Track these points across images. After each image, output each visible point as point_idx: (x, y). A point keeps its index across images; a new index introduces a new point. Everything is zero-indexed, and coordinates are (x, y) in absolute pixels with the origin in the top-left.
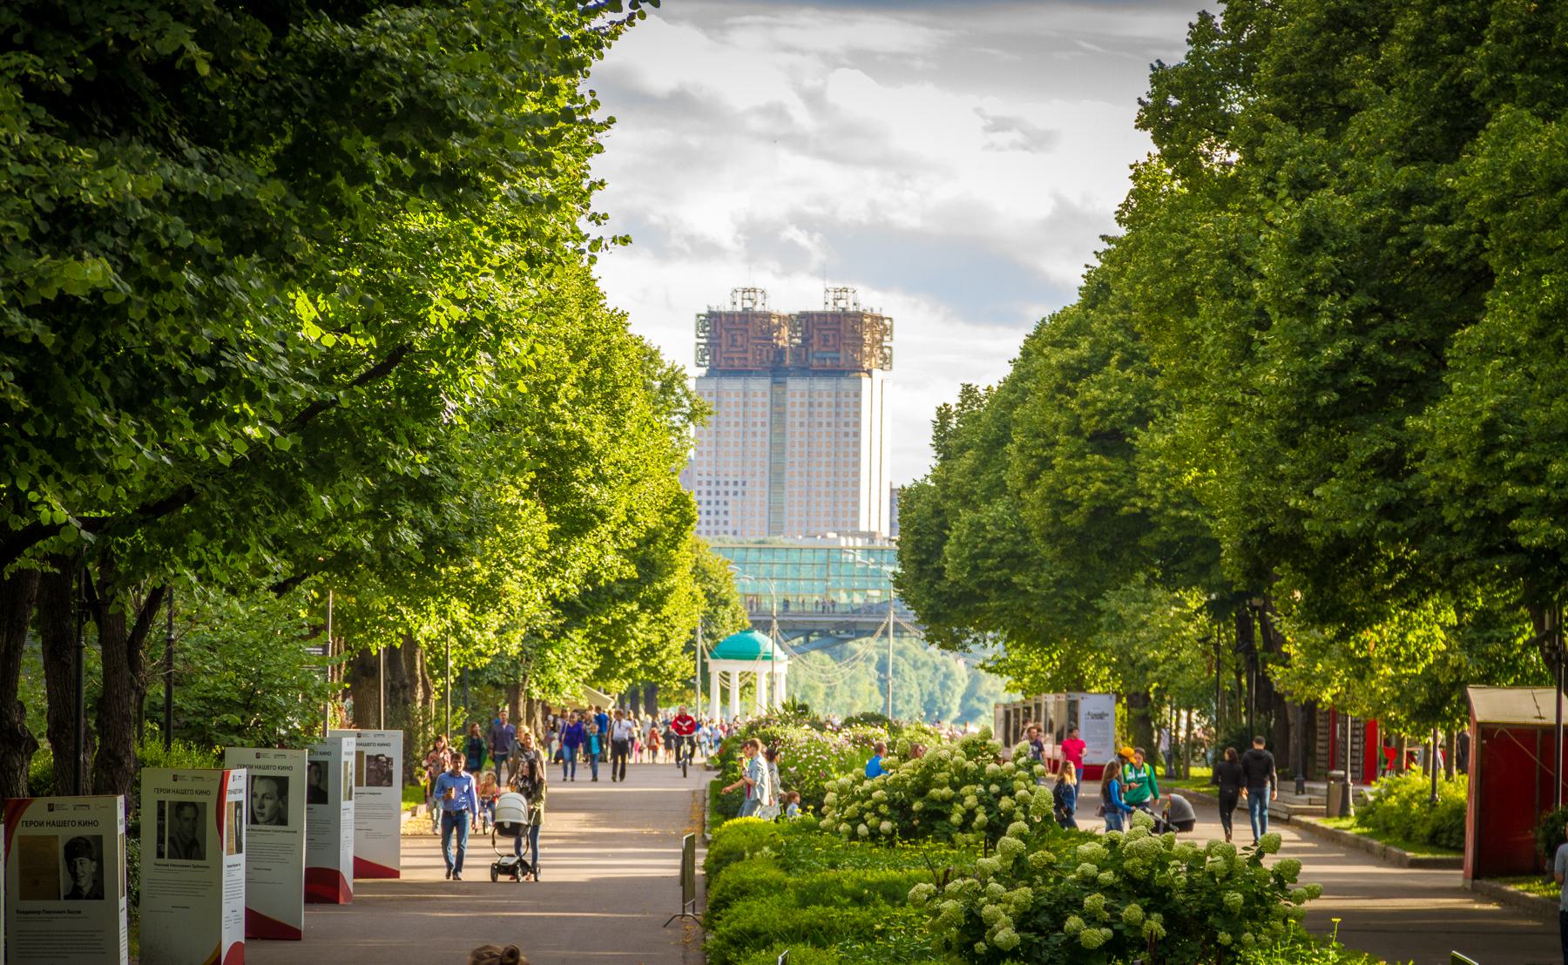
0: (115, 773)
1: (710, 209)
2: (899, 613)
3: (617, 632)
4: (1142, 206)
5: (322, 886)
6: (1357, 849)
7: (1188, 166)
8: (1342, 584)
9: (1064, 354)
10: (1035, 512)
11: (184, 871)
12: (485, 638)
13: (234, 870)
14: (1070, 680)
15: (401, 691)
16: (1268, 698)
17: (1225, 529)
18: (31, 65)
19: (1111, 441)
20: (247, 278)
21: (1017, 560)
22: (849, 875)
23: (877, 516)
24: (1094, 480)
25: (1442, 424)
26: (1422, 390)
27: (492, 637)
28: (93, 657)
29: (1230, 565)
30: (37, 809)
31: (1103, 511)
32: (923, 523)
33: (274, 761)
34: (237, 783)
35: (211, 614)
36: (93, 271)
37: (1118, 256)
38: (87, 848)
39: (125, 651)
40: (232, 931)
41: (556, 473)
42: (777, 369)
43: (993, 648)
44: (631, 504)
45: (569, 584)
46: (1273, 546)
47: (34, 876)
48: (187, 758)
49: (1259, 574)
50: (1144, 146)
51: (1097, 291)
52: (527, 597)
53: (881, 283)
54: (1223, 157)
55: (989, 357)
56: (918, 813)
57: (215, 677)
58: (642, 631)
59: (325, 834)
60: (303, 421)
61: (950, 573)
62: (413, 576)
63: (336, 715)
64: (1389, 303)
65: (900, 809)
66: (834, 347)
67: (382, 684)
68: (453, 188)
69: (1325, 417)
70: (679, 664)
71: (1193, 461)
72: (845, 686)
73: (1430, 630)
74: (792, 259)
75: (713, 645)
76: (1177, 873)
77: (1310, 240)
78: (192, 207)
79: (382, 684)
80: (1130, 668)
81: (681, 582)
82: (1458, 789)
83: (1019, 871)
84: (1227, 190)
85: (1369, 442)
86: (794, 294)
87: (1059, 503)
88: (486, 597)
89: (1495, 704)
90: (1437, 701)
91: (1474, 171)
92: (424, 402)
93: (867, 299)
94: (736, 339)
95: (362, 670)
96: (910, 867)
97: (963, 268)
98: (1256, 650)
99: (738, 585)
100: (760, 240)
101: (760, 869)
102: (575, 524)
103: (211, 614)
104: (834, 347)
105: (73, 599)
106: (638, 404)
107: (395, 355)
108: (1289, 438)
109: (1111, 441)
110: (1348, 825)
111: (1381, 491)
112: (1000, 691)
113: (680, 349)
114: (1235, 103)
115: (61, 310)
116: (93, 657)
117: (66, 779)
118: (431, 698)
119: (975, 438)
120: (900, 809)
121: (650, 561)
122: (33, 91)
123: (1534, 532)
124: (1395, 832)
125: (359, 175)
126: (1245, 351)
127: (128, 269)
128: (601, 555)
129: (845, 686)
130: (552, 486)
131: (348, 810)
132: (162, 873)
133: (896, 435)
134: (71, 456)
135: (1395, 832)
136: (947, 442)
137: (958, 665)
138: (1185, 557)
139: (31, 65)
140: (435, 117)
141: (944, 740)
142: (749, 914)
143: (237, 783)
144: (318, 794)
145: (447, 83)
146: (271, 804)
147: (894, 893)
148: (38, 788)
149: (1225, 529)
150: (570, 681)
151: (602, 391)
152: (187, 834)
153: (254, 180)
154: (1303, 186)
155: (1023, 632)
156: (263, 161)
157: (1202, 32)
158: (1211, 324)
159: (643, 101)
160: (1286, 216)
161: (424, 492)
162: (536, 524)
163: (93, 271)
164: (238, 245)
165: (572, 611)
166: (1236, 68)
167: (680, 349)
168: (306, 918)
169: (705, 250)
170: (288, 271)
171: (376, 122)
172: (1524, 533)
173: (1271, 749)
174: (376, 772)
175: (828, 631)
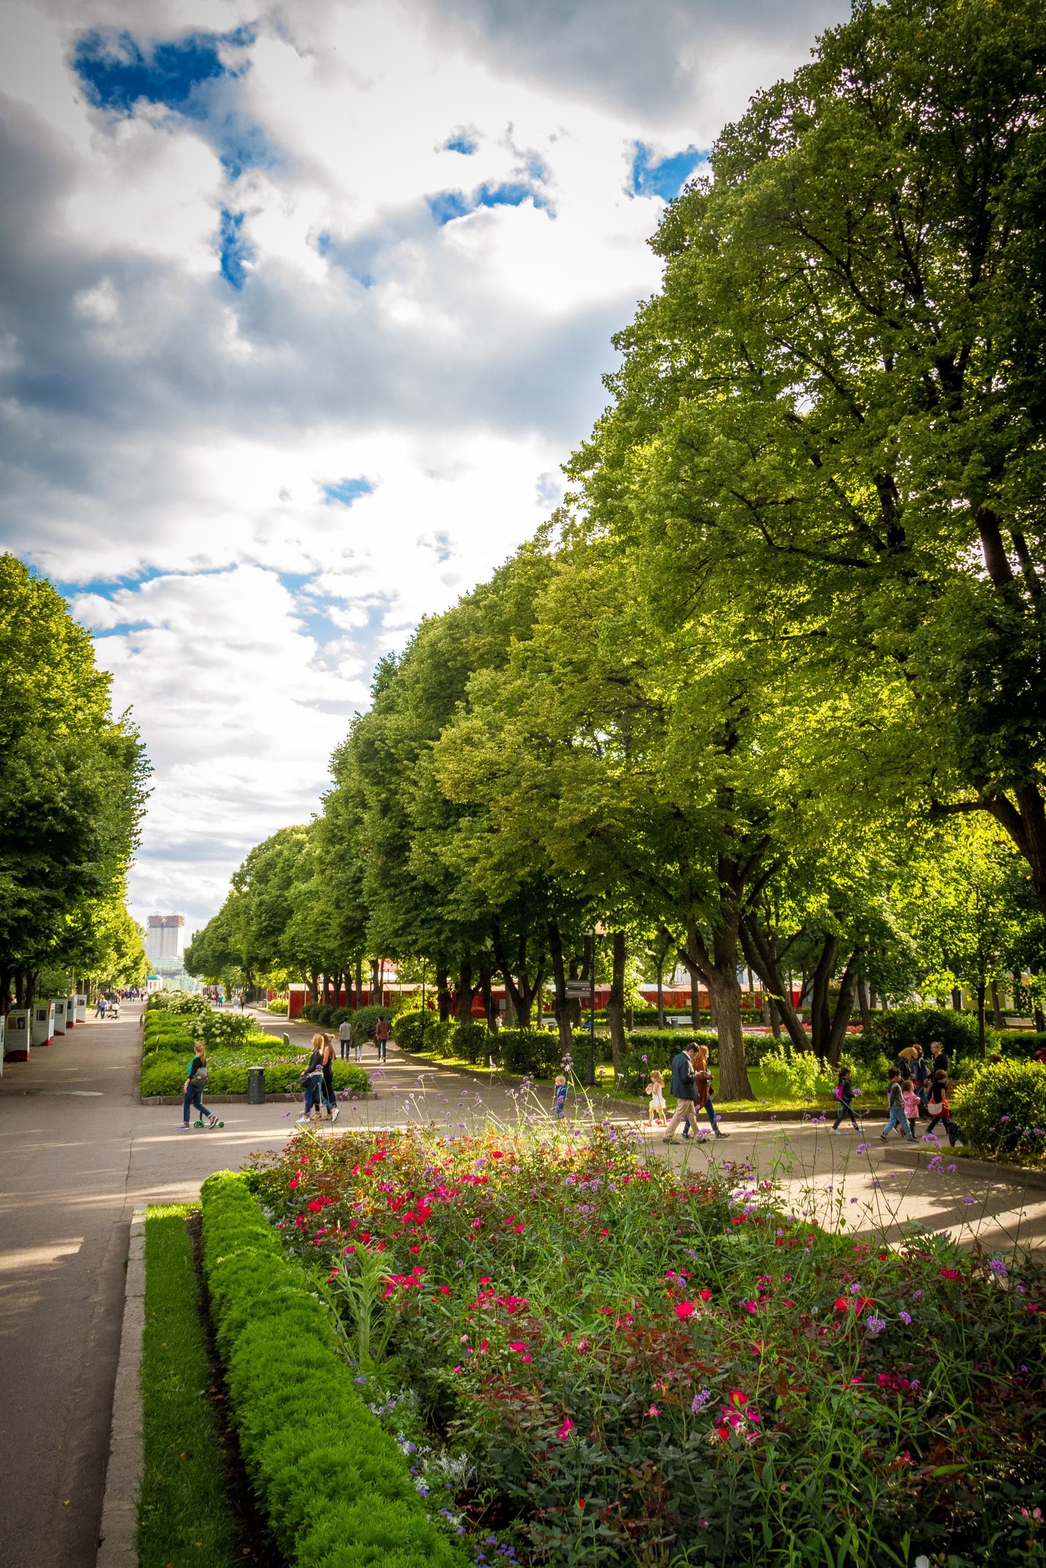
0: (28, 1005)
1: (151, 898)
2: (183, 971)
3: (130, 975)
4: (231, 899)
5: (70, 1025)
6: (268, 1013)
7: (239, 891)
8: (264, 966)
9: (216, 925)
10: (209, 953)
11: (42, 1023)
12: (104, 977)
13: (52, 1023)
14: (216, 983)
15: (87, 987)
16: (252, 986)
17: (244, 957)
18: (14, 873)
19: (224, 940)
20: (57, 912)
21: (206, 961)
22: (172, 1021)
23: (181, 953)
24: (221, 947)
25: (284, 938)
26: (280, 931)
27: (105, 977)
28: (25, 982)
29: (245, 963)
30: (12, 1012)
31: (222, 952)
32: (189, 956)
33: (61, 1001)
34: (53, 1006)
35: (47, 975)
36: (24, 912)
37: (226, 906)
38: (22, 1020)
39: (31, 981)
40: (51, 1034)
41: (118, 946)
42: (162, 926)
43: (201, 977)
44: (132, 952)
45: (120, 967)
46: (253, 959)
47: (11, 1025)
48: (43, 1001)
49: (250, 964)
50: (232, 887)
51: (222, 913)
52: (111, 969)
53: (175, 954)
54: (245, 889)
55: (202, 925)
56: (186, 1009)
57: (49, 985)
58: (134, 975)
59: (70, 1015)
60: (65, 940)
61: (194, 965)
62: (89, 967)
63: (74, 991)
64: (275, 916)
65: (182, 1008)
66: (173, 922)
67: (83, 986)
68: (99, 895)
69: (264, 936)
70: (142, 981)
71: (239, 944)
72: (174, 985)
73: (283, 974)
74: (166, 906)
75: (149, 977)
76: (233, 1020)
77: (261, 904)
78: (47, 899)
79: (83, 986)
80: (227, 981)
81: (142, 966)
82: (287, 1002)
83: (204, 1020)
84: (247, 894)
85: (272, 940)
86: (165, 913)
87: (214, 951)
88: (104, 969)
89: (294, 987)
90: (283, 987)
91: (291, 893)
92: (91, 934)
93: (179, 914)
94: (155, 922)
95: (79, 983)
96: (183, 1018)
97: (196, 908)
98: (250, 978)
99: (154, 966)
100: (160, 903)
101: (155, 1020)
102: (122, 955)
103: (47, 975)
104: (173, 922)
105: (22, 970)
106: (134, 933)
107: (87, 925)
108: (256, 940)
109: (224, 940)
110: (267, 1009)
111: (273, 949)
112: (204, 985)
113: (144, 924)
114: (248, 880)
115: (18, 919)
116: (25, 982)
117: (18, 1006)
118: (95, 989)
119: (199, 940)
120: (182, 1008)
121: (136, 962)
122: (15, 878)
123: (300, 956)
124: (275, 1010)
125: (79, 893)
126: (248, 924)
127: (33, 911)
128: (127, 961)
129: (174, 985)
130: (118, 947)
131: (75, 1011)
132: (37, 1024)
133: (184, 940)
134: (20, 946)
135: (275, 1010)
136: (194, 940)
137: (195, 980)
138: (237, 961)
139: (14, 873)
140: (94, 883)
141: (191, 996)
142: (152, 1029)
143: (53, 1006)
144: (69, 1007)
145: (97, 876)
146: (60, 1009)
147: (180, 1024)
148: (13, 1007)
149: (244, 957)
150: (121, 985)
151: (127, 931)
152: (43, 1016)
153: (59, 894)
154: (260, 894)
155: (207, 975)
156: (61, 890)
157: (242, 866)
158: (242, 919)
159: (137, 878)
160: (257, 900)
161: (91, 950)
162: (114, 955)
163: (24, 912)
164: (54, 906)
165: (121, 972)
166: (247, 873)
167: (144, 924)
168: (66, 1031)
169: (149, 905)
170: (64, 911)
171: (83, 884)
172: (102, 588)
173: (253, 995)
174: (81, 1003)
175: (171, 975)
